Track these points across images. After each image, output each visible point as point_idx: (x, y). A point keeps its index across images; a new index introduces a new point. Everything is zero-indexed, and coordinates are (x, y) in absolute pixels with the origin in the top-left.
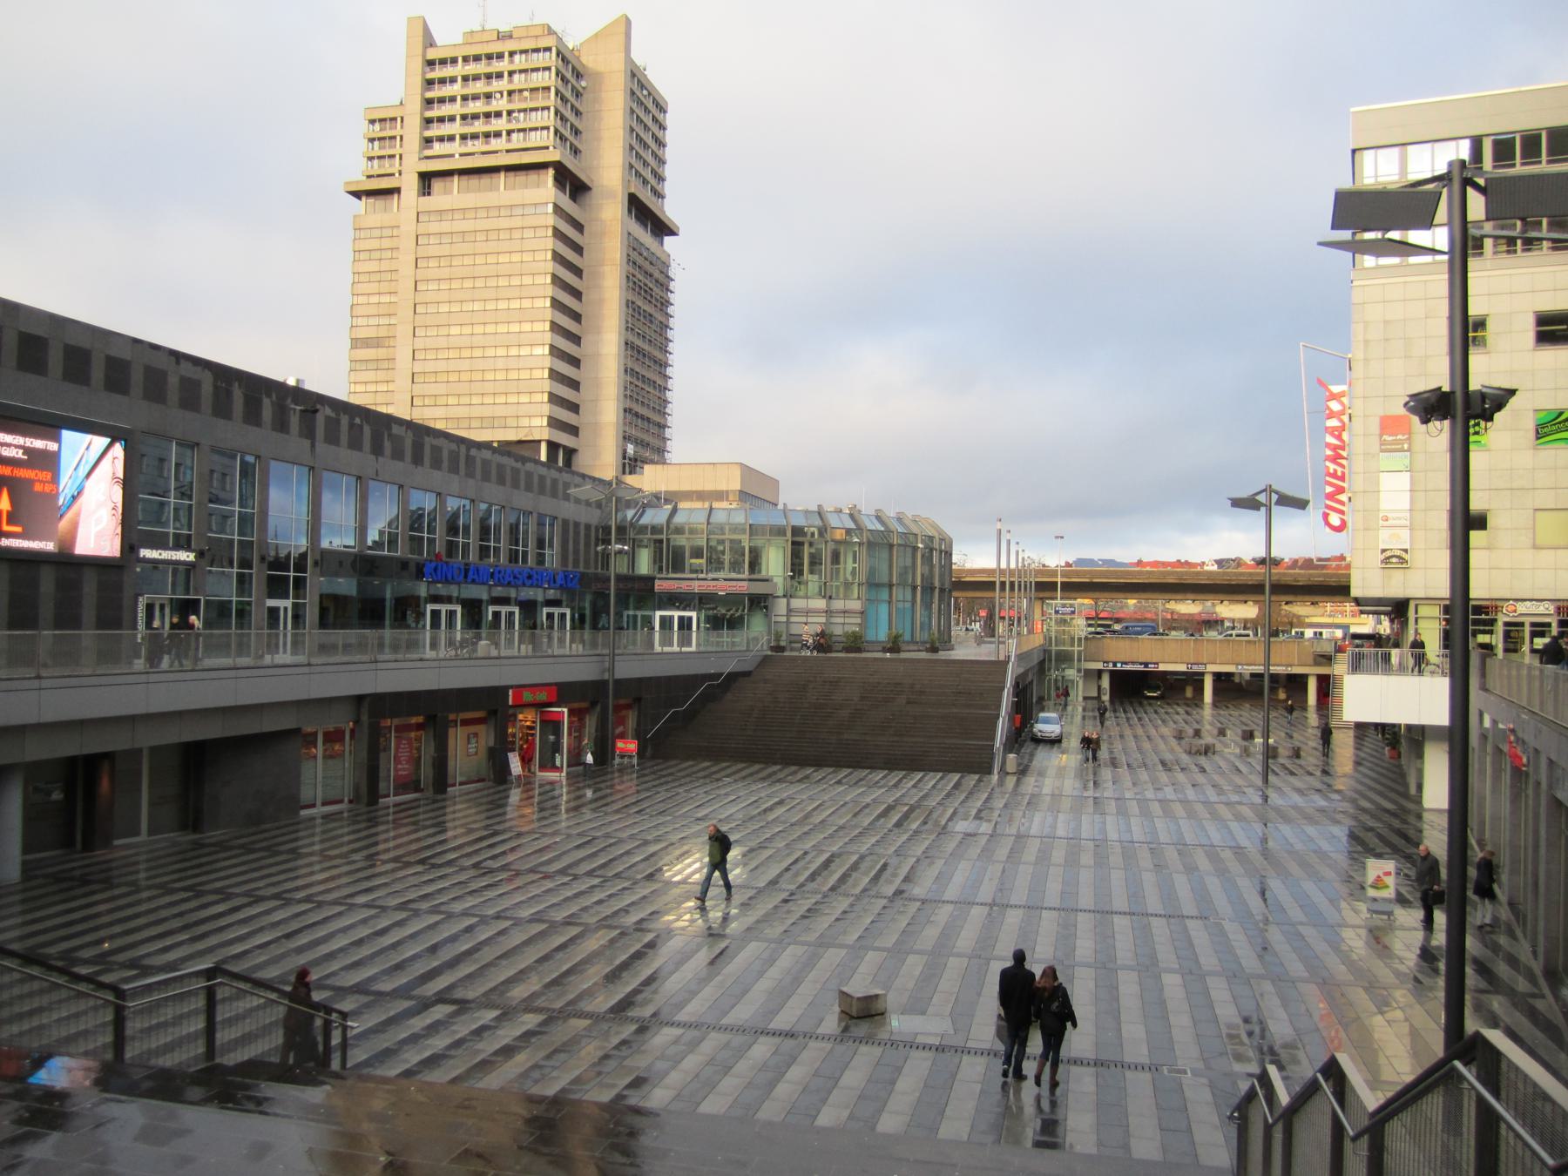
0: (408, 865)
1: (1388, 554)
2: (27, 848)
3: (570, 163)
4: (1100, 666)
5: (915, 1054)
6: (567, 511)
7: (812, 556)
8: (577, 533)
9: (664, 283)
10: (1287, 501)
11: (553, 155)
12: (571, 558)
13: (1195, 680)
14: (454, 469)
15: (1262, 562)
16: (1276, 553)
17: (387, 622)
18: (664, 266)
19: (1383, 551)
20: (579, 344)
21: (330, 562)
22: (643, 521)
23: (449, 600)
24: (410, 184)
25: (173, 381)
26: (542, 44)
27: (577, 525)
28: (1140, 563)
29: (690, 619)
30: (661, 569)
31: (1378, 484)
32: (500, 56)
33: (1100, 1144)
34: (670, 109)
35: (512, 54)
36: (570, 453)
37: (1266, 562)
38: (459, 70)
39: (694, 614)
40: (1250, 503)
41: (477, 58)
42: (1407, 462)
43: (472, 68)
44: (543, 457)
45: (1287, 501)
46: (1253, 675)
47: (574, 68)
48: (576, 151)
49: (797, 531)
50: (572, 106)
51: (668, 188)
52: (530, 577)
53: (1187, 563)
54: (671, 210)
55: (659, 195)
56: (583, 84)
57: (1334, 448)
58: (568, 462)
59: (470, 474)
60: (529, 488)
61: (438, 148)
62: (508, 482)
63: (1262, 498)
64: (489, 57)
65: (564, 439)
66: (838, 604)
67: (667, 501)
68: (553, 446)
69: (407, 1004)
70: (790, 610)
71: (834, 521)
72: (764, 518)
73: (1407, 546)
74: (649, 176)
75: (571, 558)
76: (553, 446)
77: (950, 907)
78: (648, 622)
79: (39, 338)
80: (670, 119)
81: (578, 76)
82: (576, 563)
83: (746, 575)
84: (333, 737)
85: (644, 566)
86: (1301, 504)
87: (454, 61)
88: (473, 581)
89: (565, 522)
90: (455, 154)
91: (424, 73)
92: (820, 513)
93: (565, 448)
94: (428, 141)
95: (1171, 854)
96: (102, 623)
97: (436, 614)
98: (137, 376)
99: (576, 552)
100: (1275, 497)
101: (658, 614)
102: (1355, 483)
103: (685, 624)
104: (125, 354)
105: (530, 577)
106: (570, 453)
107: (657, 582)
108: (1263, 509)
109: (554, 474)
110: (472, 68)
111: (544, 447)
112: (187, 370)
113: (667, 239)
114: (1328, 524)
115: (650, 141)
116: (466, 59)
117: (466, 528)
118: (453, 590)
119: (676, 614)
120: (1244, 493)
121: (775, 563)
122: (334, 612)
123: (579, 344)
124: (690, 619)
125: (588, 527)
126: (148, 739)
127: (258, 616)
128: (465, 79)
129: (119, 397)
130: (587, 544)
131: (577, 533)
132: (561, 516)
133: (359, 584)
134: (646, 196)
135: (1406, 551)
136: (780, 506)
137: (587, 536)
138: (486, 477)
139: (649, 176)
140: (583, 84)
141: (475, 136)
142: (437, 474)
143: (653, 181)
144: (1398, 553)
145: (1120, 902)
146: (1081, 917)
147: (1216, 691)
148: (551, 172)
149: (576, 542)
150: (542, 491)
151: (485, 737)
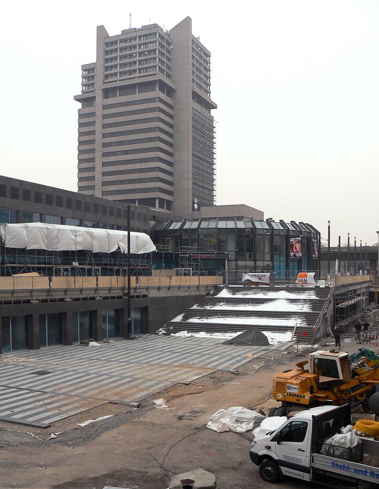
5: (126, 220)
7: (251, 257)
9: (211, 129)
13: (4, 304)
17: (121, 274)
18: (211, 119)
26: (152, 31)
32: (135, 39)
33: (80, 188)
34: (211, 55)
35: (140, 37)
38: (119, 45)
50: (167, 57)
56: (171, 47)
61: (110, 79)
64: (131, 39)
80: (212, 59)
81: (169, 44)
87: (116, 42)
90: (118, 81)
94: (107, 76)
98: (32, 195)
110: (123, 45)
115: (202, 69)
116: (121, 41)
123: (172, 185)
128: (121, 49)
134: (201, 93)
136: (265, 220)
140: (171, 47)
143: (205, 79)
148: (157, 84)
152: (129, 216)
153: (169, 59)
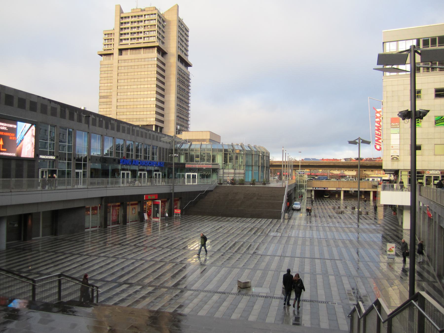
0: (115, 245)
1: (393, 157)
2: (8, 240)
3: (162, 46)
4: (311, 189)
6: (161, 145)
7: (230, 157)
8: (163, 151)
9: (188, 80)
10: (364, 142)
11: (157, 44)
12: (162, 158)
13: (338, 193)
14: (129, 133)
15: (357, 159)
16: (361, 157)
17: (110, 176)
18: (188, 75)
19: (392, 156)
20: (164, 97)
21: (94, 159)
22: (182, 148)
23: (127, 170)
24: (116, 52)
25: (49, 108)
26: (153, 12)
27: (163, 149)
28: (323, 159)
29: (195, 175)
30: (187, 161)
31: (390, 137)
32: (142, 16)
34: (190, 31)
35: (145, 15)
36: (161, 128)
37: (359, 159)
38: (130, 20)
39: (196, 174)
40: (354, 143)
41: (135, 17)
42: (398, 131)
43: (134, 19)
44: (154, 130)
45: (364, 142)
46: (355, 191)
47: (162, 19)
48: (163, 43)
49: (226, 150)
50: (162, 30)
51: (189, 53)
52: (150, 163)
53: (336, 159)
54: (190, 59)
55: (187, 55)
56: (165, 24)
57: (378, 127)
58: (161, 131)
59: (133, 134)
60: (150, 138)
61: (124, 42)
62: (144, 137)
63: (357, 141)
64: (139, 16)
65: (160, 124)
66: (237, 171)
67: (189, 142)
68: (157, 126)
69: (115, 284)
70: (224, 173)
71: (236, 148)
72: (216, 147)
73: (398, 155)
74: (184, 50)
75: (162, 158)
76: (157, 126)
77: (269, 257)
78: (184, 176)
79: (11, 96)
80: (190, 34)
81: (164, 21)
82: (163, 159)
83: (211, 163)
84: (94, 209)
85: (182, 160)
86: (368, 143)
87: (129, 17)
88: (134, 165)
89: (160, 148)
90: (129, 44)
91: (120, 21)
92: (232, 145)
93: (160, 127)
94: (121, 40)
95: (332, 242)
96: (29, 177)
97: (123, 174)
98: (39, 107)
99: (163, 156)
100: (361, 141)
101: (186, 174)
102: (384, 137)
103: (194, 177)
104: (35, 100)
105: (150, 163)
106: (161, 128)
107: (186, 165)
108: (358, 144)
109: (157, 134)
110: (134, 19)
111: (154, 127)
112: (53, 105)
113: (189, 68)
114: (376, 148)
115: (184, 40)
116: (132, 17)
117: (132, 150)
118: (128, 167)
119: (191, 174)
120: (352, 140)
121: (219, 159)
122: (94, 173)
123: (164, 97)
124: (195, 175)
125: (166, 149)
126: (42, 209)
127: (73, 174)
128: (132, 22)
129: (34, 112)
130: (166, 154)
131: (163, 151)
132: (159, 146)
133: (102, 166)
134: (183, 56)
135: (398, 156)
136: (221, 143)
137: (166, 152)
138: (138, 135)
139: (184, 50)
140: (165, 24)
141: (134, 39)
142: (124, 134)
143: (185, 51)
144: (396, 157)
145: (317, 256)
146: (306, 260)
147: (344, 196)
148: (156, 49)
149: (163, 154)
150: (153, 139)
151: (137, 209)
152: (195, 271)
153: (164, 32)
